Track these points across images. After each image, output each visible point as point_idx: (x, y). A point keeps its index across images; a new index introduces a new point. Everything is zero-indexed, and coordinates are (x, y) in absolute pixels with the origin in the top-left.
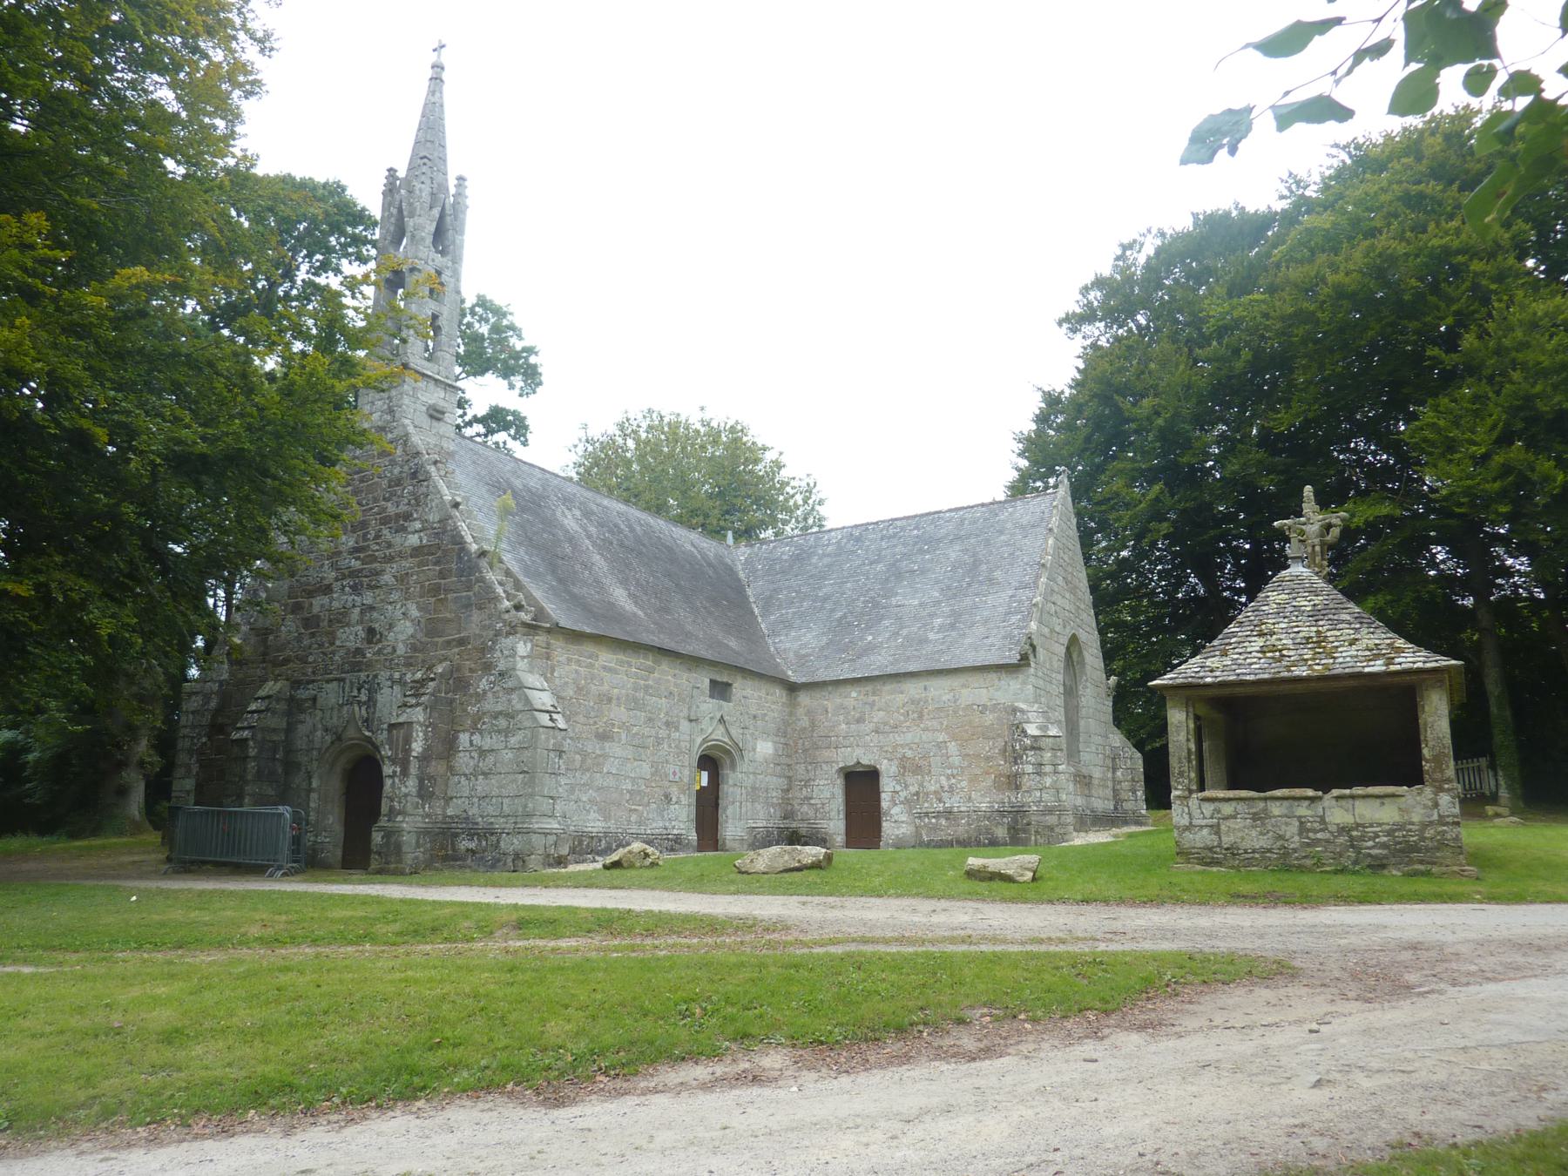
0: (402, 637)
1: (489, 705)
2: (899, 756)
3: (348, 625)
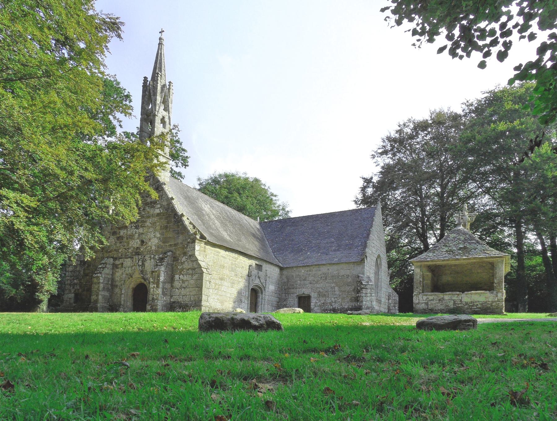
0: (154, 244)
1: (186, 266)
2: (318, 291)
3: (134, 239)
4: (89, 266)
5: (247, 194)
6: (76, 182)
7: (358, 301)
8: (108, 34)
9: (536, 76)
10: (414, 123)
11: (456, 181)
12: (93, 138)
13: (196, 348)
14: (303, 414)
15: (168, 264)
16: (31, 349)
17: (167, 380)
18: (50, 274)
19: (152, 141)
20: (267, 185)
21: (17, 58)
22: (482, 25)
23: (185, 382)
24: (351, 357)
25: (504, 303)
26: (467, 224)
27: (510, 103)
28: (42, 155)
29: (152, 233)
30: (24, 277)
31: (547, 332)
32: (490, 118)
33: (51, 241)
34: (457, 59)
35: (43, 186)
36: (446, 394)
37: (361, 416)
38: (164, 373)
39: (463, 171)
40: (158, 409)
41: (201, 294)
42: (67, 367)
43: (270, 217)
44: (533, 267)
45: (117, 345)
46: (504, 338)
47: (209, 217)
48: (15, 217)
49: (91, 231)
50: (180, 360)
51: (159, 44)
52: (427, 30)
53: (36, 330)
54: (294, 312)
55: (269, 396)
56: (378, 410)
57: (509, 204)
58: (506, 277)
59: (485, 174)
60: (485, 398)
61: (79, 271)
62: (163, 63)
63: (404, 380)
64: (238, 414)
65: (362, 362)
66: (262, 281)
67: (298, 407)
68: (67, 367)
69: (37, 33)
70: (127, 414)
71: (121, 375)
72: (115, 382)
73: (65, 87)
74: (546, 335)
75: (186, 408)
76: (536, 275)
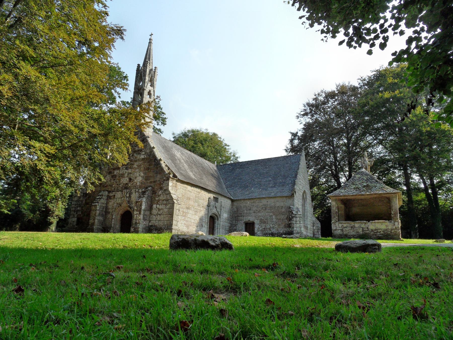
0: (139, 181)
1: (162, 198)
3: (124, 177)
4: (89, 197)
5: (208, 144)
6: (85, 136)
7: (290, 227)
8: (115, 37)
9: (407, 60)
10: (326, 93)
11: (357, 135)
12: (100, 105)
13: (167, 263)
14: (249, 322)
15: (148, 196)
16: (40, 261)
17: (143, 289)
18: (60, 203)
19: (141, 108)
20: (222, 138)
21: (51, 53)
22: (368, 25)
23: (157, 290)
24: (286, 273)
25: (400, 230)
26: (368, 167)
27: (391, 78)
28: (62, 117)
29: (138, 173)
30: (41, 205)
31: (435, 256)
32: (378, 89)
33: (63, 178)
34: (352, 49)
35: (61, 138)
36: (361, 308)
37: (295, 324)
38: (142, 283)
39: (362, 127)
40: (135, 313)
41: (172, 220)
42: (67, 276)
43: (225, 162)
44: (419, 202)
45: (106, 259)
46: (403, 260)
47: (180, 161)
48: (38, 160)
49: (94, 171)
50: (154, 273)
51: (149, 43)
52: (331, 30)
53: (45, 246)
54: (242, 236)
55: (223, 305)
56: (309, 320)
57: (397, 152)
58: (400, 209)
59: (377, 129)
60: (393, 312)
61: (82, 201)
62: (151, 55)
63: (328, 294)
64: (199, 319)
65: (295, 278)
66: (218, 210)
67: (246, 315)
68: (67, 276)
69: (66, 37)
70: (111, 317)
71: (108, 284)
72: (103, 289)
73: (83, 72)
74: (435, 258)
75: (157, 313)
76: (422, 208)
